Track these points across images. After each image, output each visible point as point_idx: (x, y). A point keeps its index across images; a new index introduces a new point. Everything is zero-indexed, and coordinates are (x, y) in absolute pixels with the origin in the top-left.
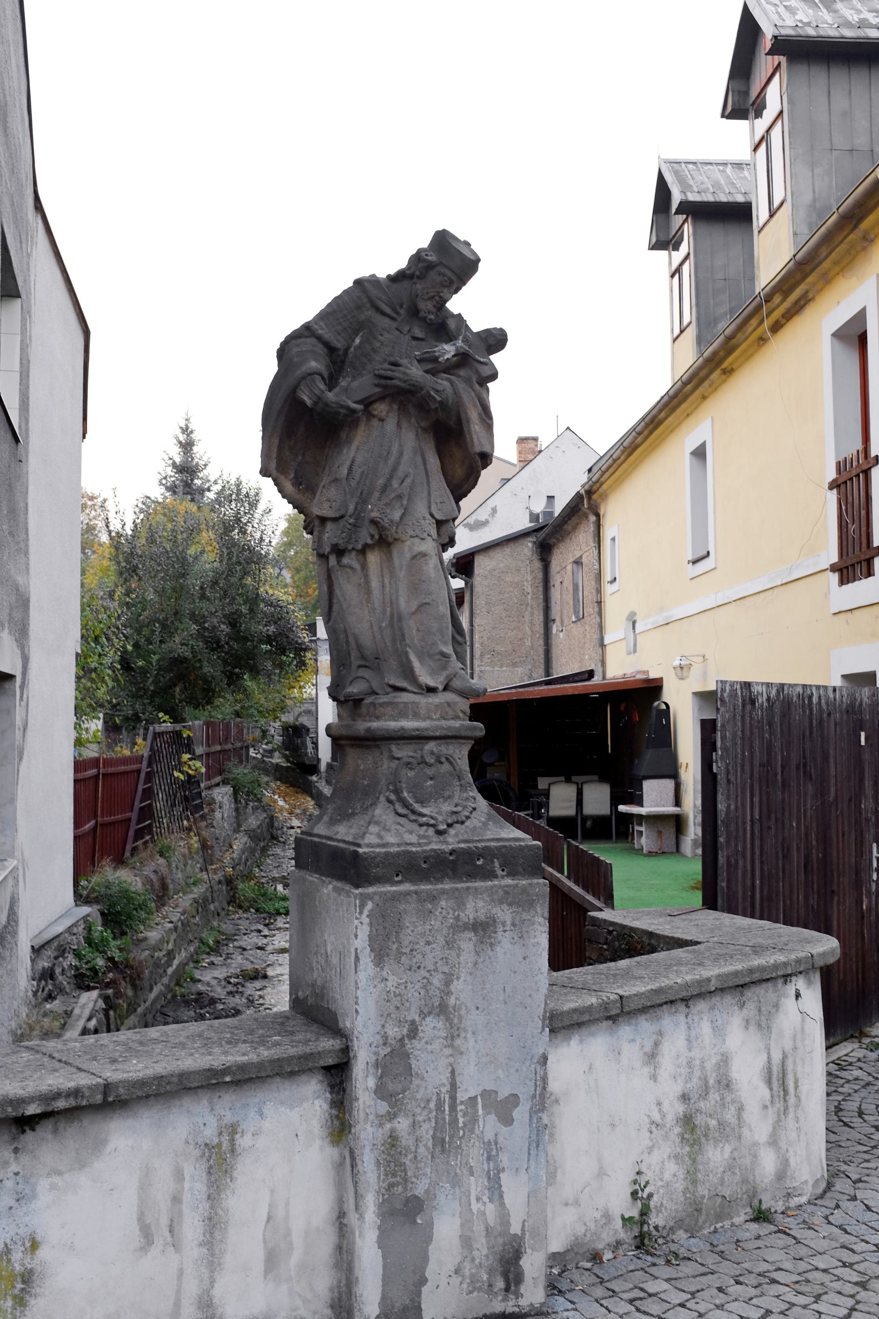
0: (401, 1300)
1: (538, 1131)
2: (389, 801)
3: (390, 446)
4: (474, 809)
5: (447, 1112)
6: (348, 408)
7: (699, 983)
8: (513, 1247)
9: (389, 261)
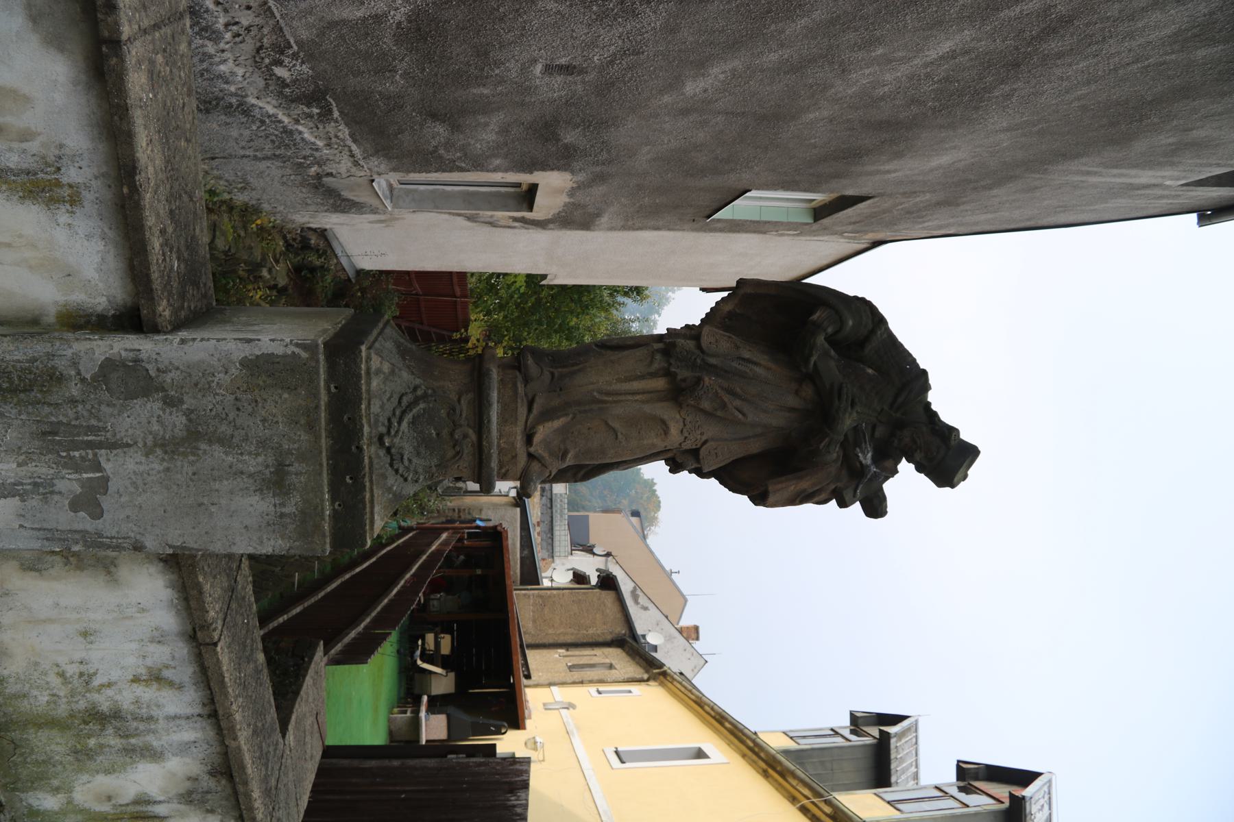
1: (64, 540)
2: (415, 388)
3: (771, 405)
4: (406, 480)
6: (811, 355)
7: (232, 729)
9: (945, 401)
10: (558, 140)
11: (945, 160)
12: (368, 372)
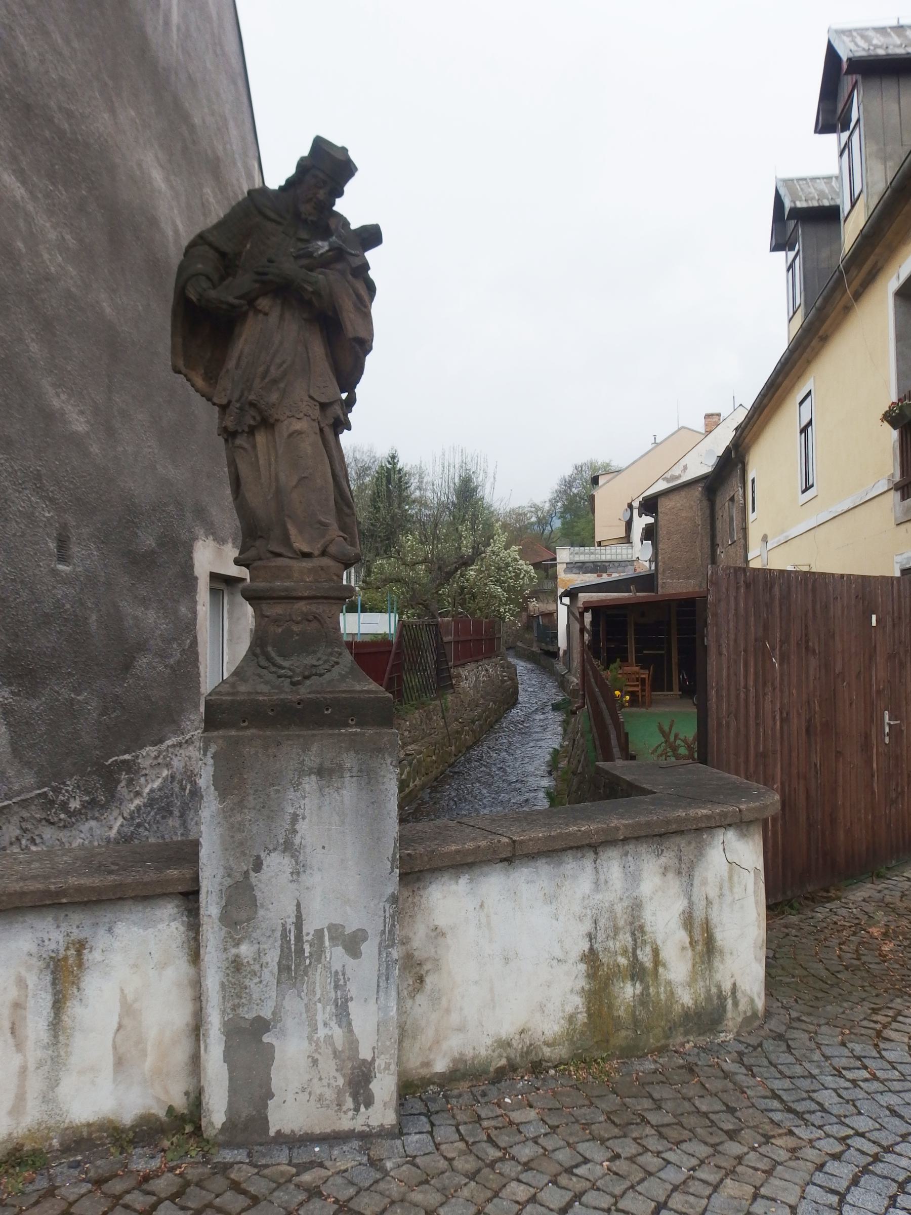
0: (246, 1112)
4: (337, 663)
5: (293, 942)
8: (363, 1072)
10: (153, 552)
11: (157, 176)
12: (233, 694)
